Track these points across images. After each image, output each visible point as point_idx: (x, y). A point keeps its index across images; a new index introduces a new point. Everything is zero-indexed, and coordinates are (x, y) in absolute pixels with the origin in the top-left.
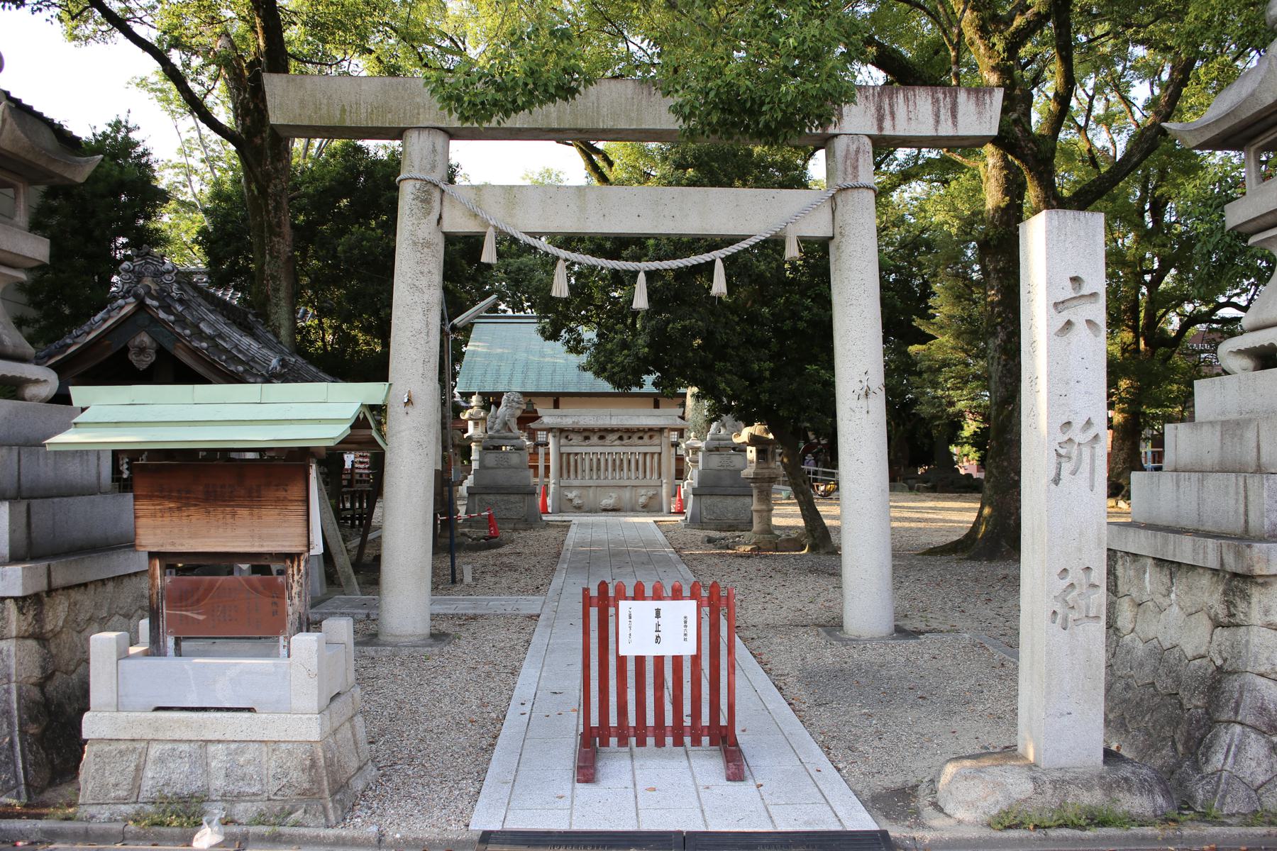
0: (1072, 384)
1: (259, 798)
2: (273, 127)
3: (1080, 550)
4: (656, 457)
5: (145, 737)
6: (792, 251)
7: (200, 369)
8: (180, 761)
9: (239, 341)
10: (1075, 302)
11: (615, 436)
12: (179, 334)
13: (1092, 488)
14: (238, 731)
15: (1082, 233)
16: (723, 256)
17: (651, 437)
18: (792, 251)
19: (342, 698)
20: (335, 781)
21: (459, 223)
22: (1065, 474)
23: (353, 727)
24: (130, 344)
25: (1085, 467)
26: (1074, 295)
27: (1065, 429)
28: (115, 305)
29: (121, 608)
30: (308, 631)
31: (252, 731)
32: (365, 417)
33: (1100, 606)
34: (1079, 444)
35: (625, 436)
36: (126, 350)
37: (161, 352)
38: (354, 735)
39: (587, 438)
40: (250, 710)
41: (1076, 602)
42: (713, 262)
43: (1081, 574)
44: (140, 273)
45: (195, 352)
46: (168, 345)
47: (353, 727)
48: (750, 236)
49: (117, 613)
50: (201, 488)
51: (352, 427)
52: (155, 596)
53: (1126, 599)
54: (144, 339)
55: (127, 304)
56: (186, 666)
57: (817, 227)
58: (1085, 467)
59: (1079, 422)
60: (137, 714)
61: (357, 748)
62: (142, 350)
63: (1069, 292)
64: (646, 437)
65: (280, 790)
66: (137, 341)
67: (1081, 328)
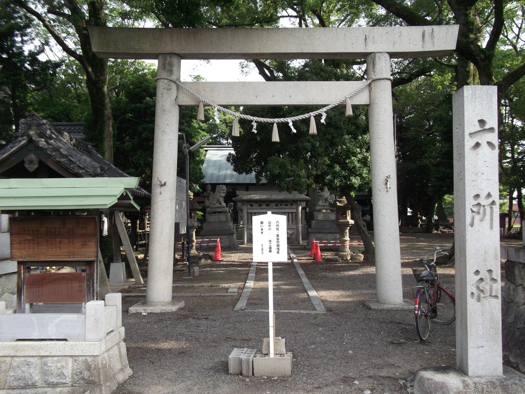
0: (479, 175)
1: (67, 385)
2: (93, 52)
3: (485, 260)
4: (294, 215)
5: (10, 355)
6: (349, 112)
7: (60, 172)
8: (28, 366)
9: (80, 158)
10: (481, 133)
11: (274, 204)
12: (49, 154)
13: (492, 228)
14: (58, 351)
15: (485, 97)
16: (315, 115)
17: (291, 205)
18: (349, 112)
19: (113, 333)
20: (107, 376)
21: (187, 101)
22: (476, 221)
23: (119, 348)
24: (25, 159)
25: (488, 217)
26: (480, 129)
27: (476, 198)
28: (17, 140)
29: (9, 290)
30: (97, 299)
31: (65, 351)
32: (127, 194)
33: (498, 290)
34: (484, 206)
35: (279, 204)
36: (23, 162)
37: (41, 163)
38: (120, 352)
39: (260, 205)
40: (65, 340)
41: (484, 287)
42: (310, 118)
43: (487, 274)
44: (30, 124)
45: (58, 163)
46: (43, 160)
47: (119, 348)
48: (328, 105)
49: (7, 292)
50: (44, 229)
51: (118, 199)
52: (20, 283)
53: (520, 287)
54: (32, 156)
55: (23, 140)
56: (33, 318)
57: (362, 99)
58: (488, 217)
59: (483, 194)
60: (7, 343)
61: (121, 359)
62: (31, 162)
63: (478, 128)
64: (284, 204)
65: (78, 381)
66: (29, 157)
67: (484, 147)
